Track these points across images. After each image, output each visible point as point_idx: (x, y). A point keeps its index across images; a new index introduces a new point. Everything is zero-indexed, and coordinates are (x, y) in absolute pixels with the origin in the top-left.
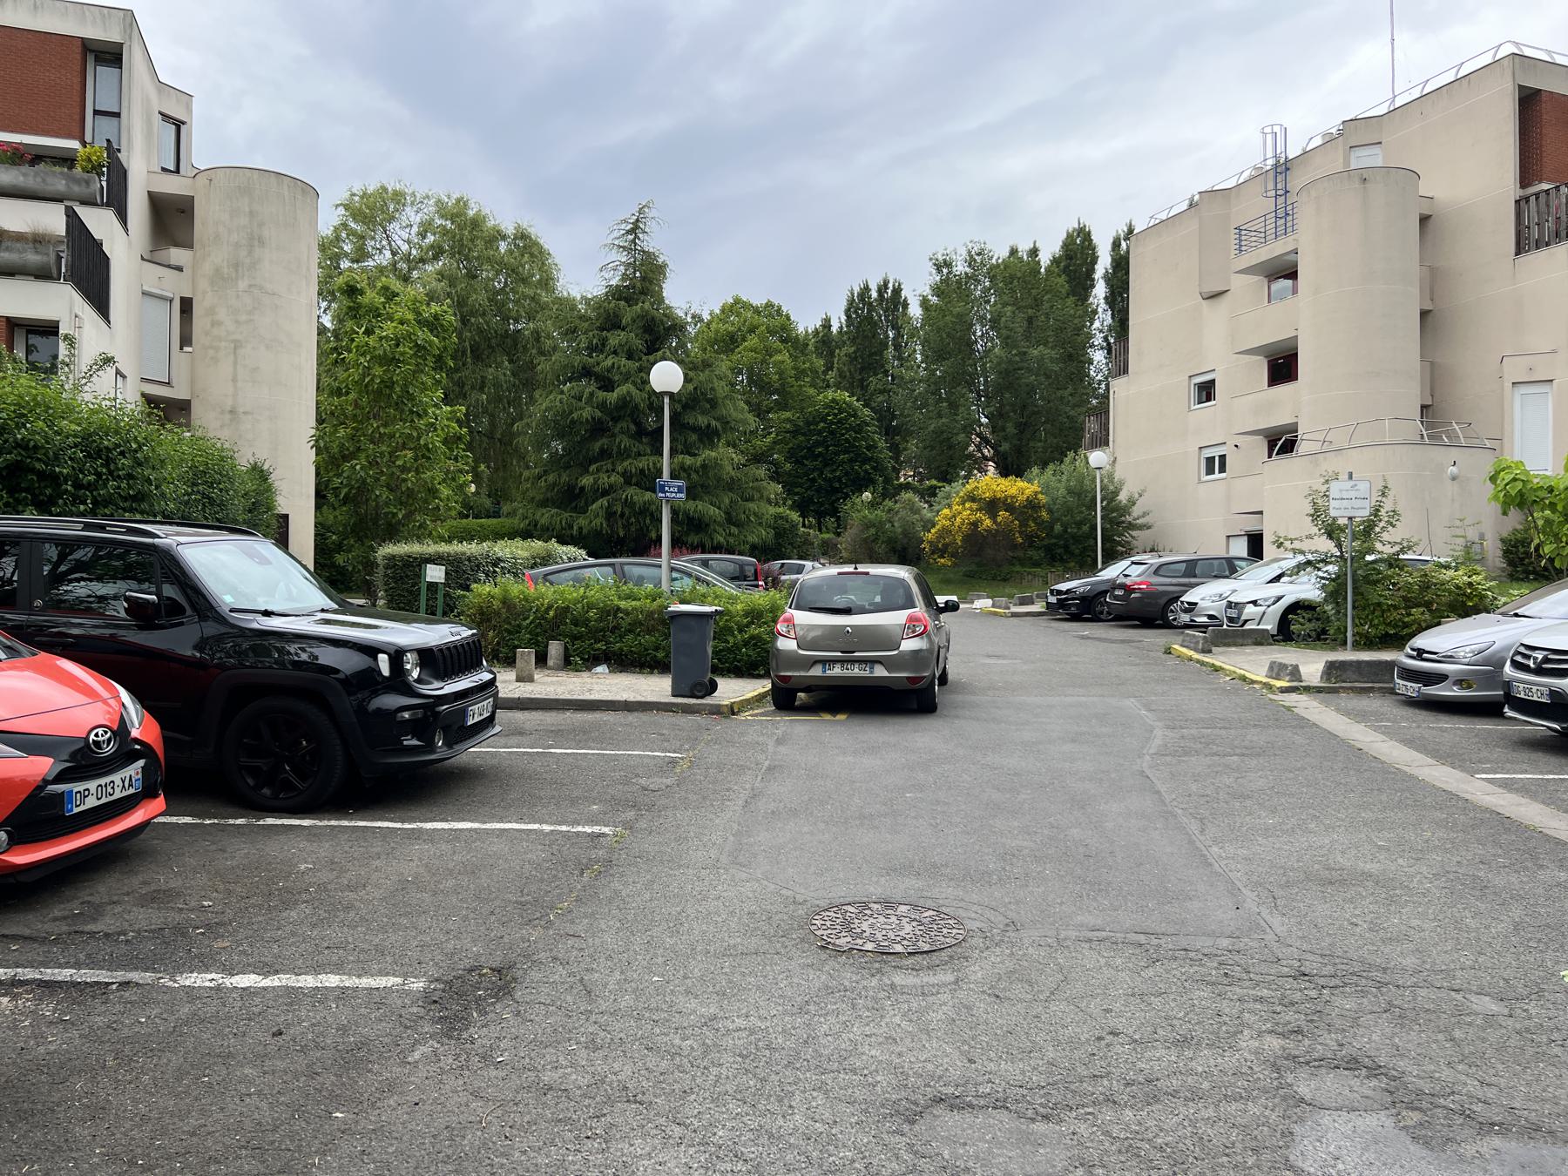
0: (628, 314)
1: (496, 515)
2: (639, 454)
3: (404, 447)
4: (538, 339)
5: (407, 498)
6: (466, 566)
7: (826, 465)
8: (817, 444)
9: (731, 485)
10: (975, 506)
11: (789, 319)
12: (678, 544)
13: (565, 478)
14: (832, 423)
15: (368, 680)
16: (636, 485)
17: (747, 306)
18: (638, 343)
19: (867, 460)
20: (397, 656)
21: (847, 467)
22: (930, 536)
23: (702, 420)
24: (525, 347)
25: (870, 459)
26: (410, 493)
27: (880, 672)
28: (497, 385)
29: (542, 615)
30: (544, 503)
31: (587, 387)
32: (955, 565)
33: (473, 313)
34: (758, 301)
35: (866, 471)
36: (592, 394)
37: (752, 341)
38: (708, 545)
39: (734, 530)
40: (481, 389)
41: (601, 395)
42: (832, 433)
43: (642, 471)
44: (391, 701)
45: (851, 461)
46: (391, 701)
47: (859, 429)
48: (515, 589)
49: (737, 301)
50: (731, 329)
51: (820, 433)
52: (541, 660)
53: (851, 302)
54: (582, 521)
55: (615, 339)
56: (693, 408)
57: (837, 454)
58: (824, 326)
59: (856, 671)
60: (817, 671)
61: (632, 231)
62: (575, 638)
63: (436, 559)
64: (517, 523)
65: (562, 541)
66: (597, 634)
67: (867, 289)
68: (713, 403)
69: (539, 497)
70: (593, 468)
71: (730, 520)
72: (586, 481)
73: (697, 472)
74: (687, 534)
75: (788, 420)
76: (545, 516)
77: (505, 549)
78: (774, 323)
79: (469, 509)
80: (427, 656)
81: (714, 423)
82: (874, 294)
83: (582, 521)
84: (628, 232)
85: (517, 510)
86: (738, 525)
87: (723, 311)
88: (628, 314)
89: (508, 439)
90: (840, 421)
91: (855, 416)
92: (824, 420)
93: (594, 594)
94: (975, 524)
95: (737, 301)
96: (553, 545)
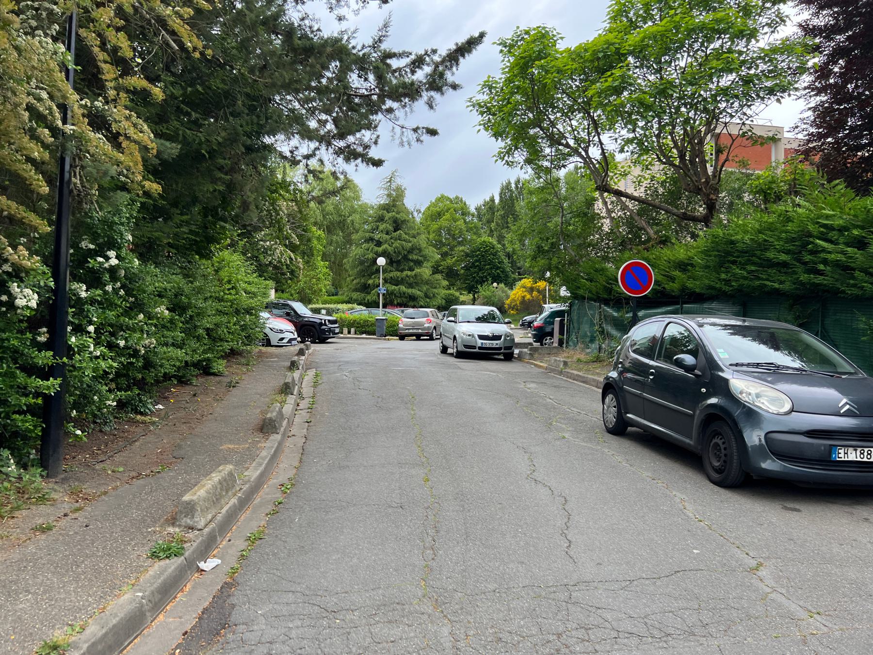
0: (388, 216)
1: (336, 295)
2: (391, 271)
3: (313, 278)
4: (353, 224)
5: (314, 292)
6: (330, 311)
7: (480, 270)
8: (477, 261)
9: (427, 283)
10: (524, 290)
11: (465, 204)
12: (384, 306)
13: (363, 281)
14: (483, 252)
15: (321, 324)
16: (390, 283)
17: (448, 199)
18: (391, 228)
19: (498, 268)
20: (325, 321)
21: (489, 271)
22: (508, 302)
23: (415, 257)
24: (348, 227)
25: (500, 268)
26: (315, 291)
27: (420, 331)
28: (337, 242)
29: (349, 322)
30: (356, 290)
31: (371, 245)
32: (517, 313)
33: (328, 214)
34: (452, 196)
35: (498, 273)
36: (372, 249)
37: (448, 216)
38: (417, 305)
39: (428, 300)
40: (331, 245)
41: (376, 248)
42: (483, 256)
43: (391, 277)
44: (324, 327)
45: (491, 268)
46: (324, 327)
47: (495, 254)
48: (343, 316)
49: (443, 196)
50: (438, 210)
51: (477, 256)
52: (349, 332)
53: (502, 189)
54: (369, 297)
55: (382, 226)
56: (412, 253)
57: (485, 265)
58: (491, 200)
59: (415, 331)
60: (407, 331)
61: (390, 181)
62: (357, 327)
63: (324, 308)
64: (345, 298)
65: (359, 304)
66: (362, 326)
67: (509, 183)
68: (420, 250)
69: (353, 287)
70: (373, 276)
71: (427, 296)
72: (370, 282)
73: (412, 277)
74: (409, 302)
75: (463, 251)
76: (355, 295)
77: (340, 306)
78: (460, 208)
79: (330, 294)
80: (329, 321)
81: (420, 258)
82: (513, 186)
83: (369, 297)
84: (387, 182)
85: (344, 294)
86: (429, 298)
87: (436, 201)
88: (388, 216)
89: (341, 265)
90: (486, 251)
91: (493, 248)
92: (479, 250)
93: (363, 317)
94: (524, 297)
95: (443, 196)
96: (355, 306)
